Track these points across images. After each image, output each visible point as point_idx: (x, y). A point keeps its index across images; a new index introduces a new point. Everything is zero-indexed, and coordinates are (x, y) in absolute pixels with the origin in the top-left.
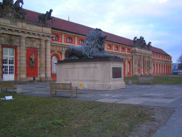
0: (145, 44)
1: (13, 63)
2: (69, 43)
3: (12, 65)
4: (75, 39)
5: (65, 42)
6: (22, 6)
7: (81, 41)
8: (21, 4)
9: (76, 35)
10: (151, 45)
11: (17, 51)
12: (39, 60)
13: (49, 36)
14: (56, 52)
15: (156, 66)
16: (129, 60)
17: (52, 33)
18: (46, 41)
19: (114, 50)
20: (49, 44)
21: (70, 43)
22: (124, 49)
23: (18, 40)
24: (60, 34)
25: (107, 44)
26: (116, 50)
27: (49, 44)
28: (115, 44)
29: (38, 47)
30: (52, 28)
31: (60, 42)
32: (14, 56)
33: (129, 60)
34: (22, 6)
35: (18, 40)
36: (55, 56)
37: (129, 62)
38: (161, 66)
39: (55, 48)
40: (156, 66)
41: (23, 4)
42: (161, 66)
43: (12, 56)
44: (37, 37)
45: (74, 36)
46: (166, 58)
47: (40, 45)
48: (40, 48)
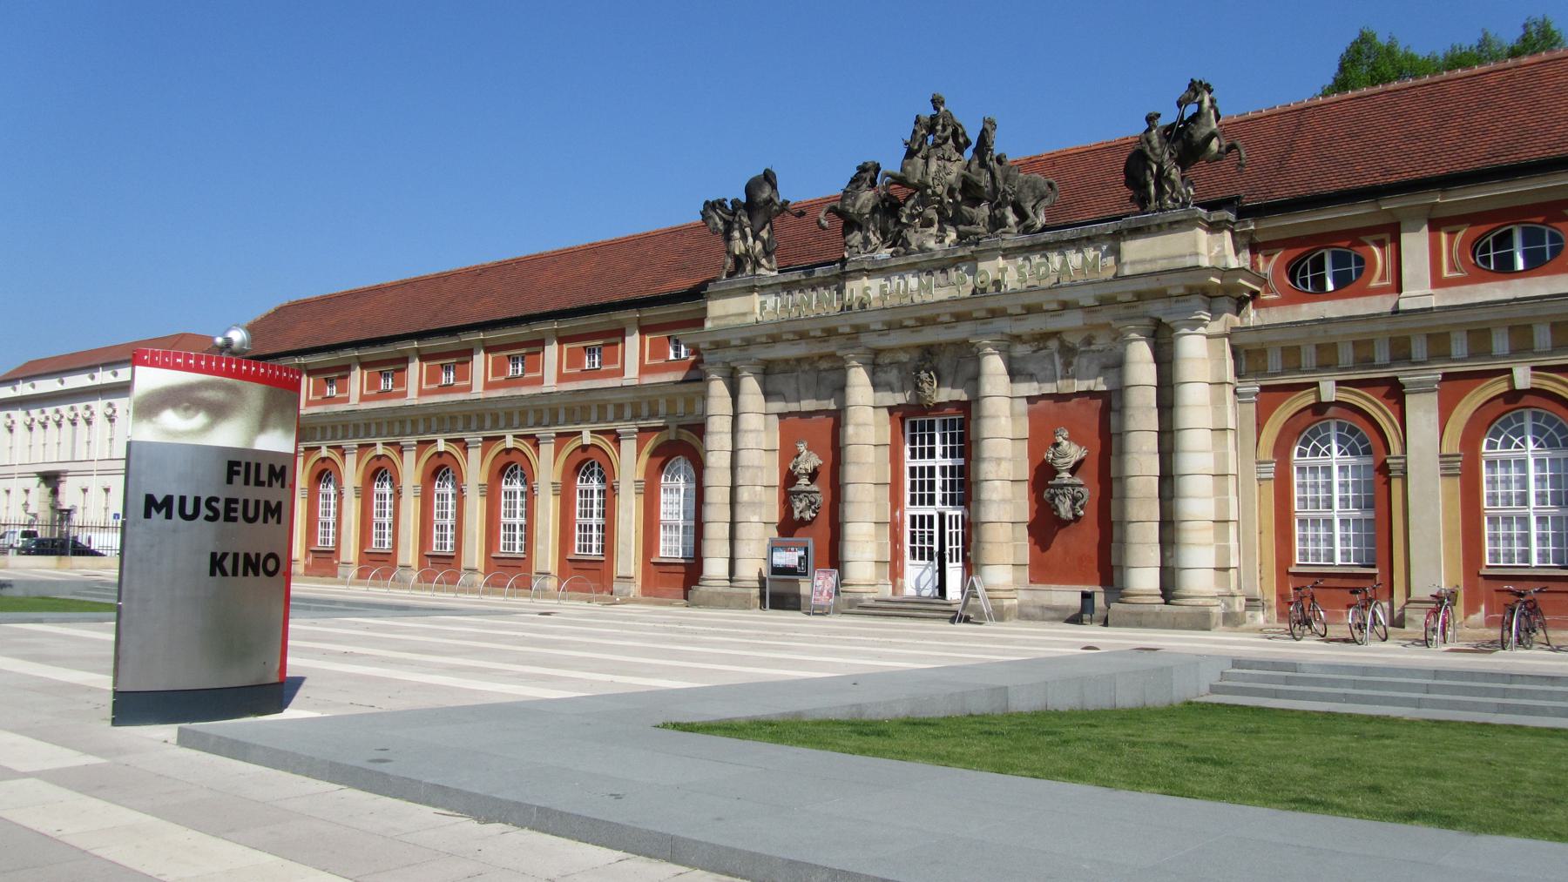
5: (1438, 282)
41: (774, 187)
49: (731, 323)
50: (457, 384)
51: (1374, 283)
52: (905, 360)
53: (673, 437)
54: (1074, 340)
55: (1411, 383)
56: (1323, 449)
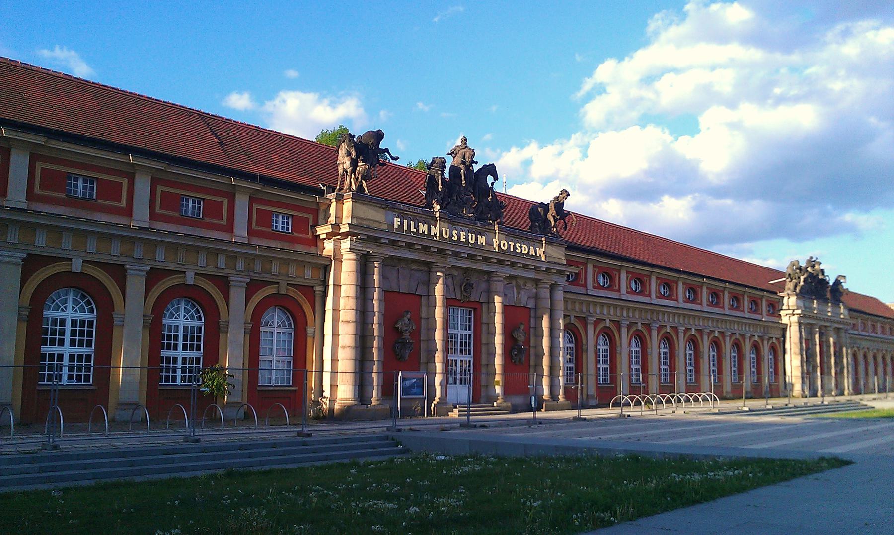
0: (824, 282)
1: (198, 349)
2: (603, 288)
3: (84, 351)
4: (677, 286)
6: (492, 184)
7: (635, 282)
8: (490, 179)
9: (624, 264)
10: (845, 286)
11: (481, 316)
12: (532, 343)
13: (560, 273)
14: (190, 279)
15: (749, 355)
16: (738, 336)
17: (567, 261)
18: (553, 287)
19: (726, 308)
20: (559, 295)
21: (608, 289)
22: (670, 288)
23: (483, 286)
24: (616, 270)
25: (684, 284)
26: (688, 300)
27: (559, 295)
28: (732, 287)
29: (531, 305)
30: (571, 247)
31: (741, 311)
32: (471, 332)
33: (738, 336)
34: (492, 184)
35: (483, 286)
36: (285, 309)
37: (736, 344)
38: (879, 359)
39: (67, 243)
40: (749, 355)
41: (496, 178)
42: (879, 359)
43: (468, 332)
44: (532, 275)
45: (648, 274)
46: (879, 330)
47: (537, 297)
48: (536, 309)
49: (370, 225)
50: (101, 202)
51: (580, 282)
52: (455, 274)
53: (283, 292)
54: (521, 283)
55: (233, 281)
56: (62, 307)
